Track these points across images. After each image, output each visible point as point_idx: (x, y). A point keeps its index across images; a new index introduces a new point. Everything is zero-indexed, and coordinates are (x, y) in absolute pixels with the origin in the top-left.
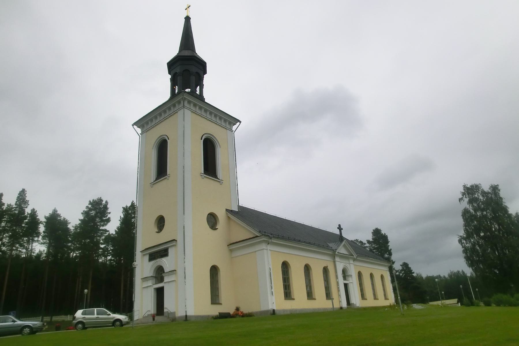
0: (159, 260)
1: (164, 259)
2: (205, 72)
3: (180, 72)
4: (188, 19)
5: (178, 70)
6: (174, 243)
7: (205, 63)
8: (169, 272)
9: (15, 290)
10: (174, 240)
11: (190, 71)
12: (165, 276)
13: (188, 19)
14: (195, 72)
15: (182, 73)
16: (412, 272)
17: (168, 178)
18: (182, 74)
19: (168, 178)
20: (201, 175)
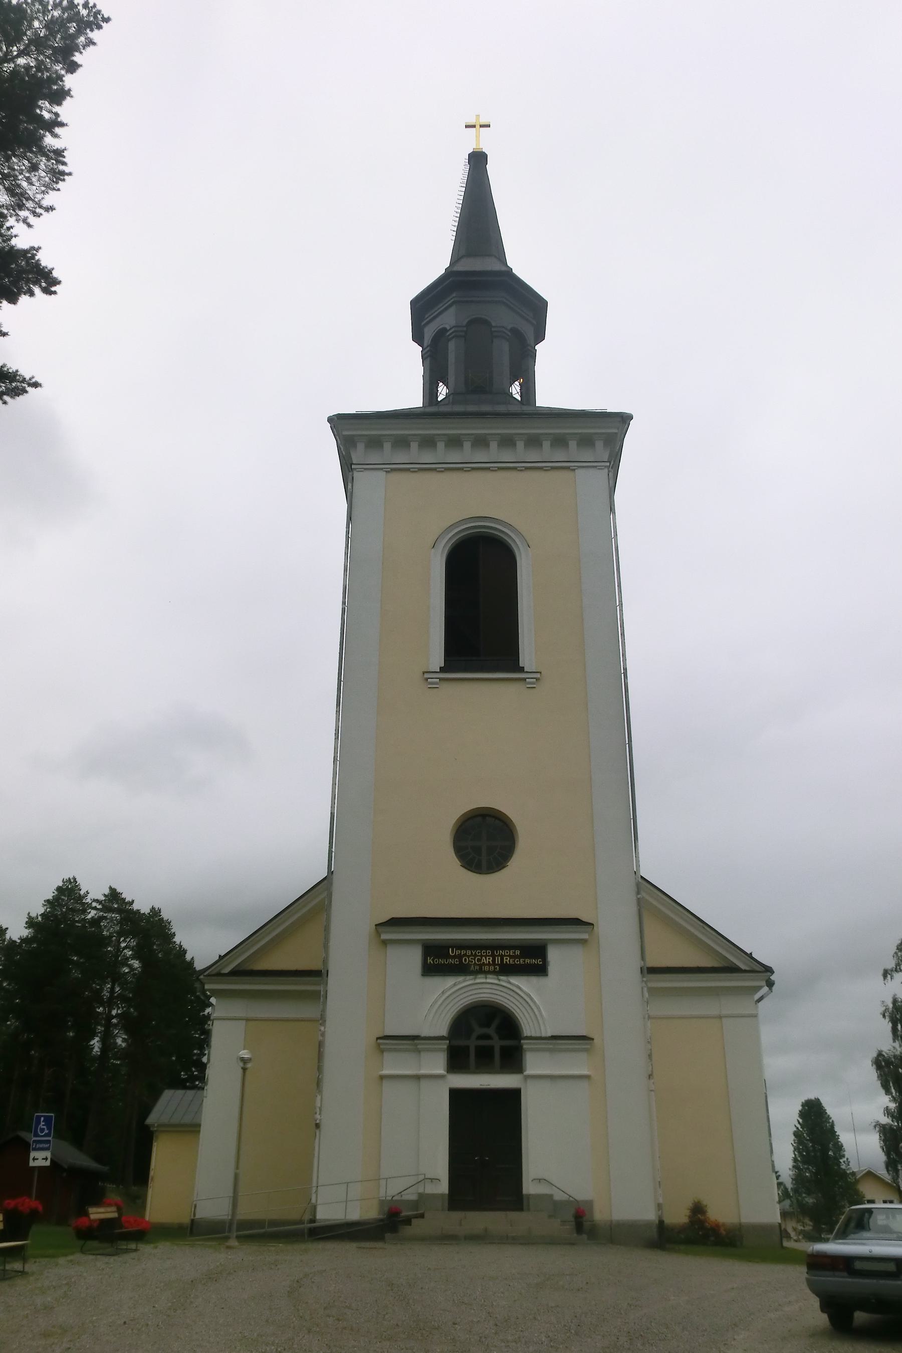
0: (488, 981)
1: (523, 984)
2: (540, 336)
3: (454, 327)
4: (478, 160)
5: (448, 319)
6: (586, 932)
7: (545, 303)
8: (554, 1038)
9: (174, 1058)
10: (576, 922)
11: (493, 324)
12: (532, 1050)
13: (478, 160)
14: (509, 328)
15: (465, 329)
16: (126, 901)
17: (533, 683)
18: (463, 334)
19: (533, 683)
20: (427, 679)
